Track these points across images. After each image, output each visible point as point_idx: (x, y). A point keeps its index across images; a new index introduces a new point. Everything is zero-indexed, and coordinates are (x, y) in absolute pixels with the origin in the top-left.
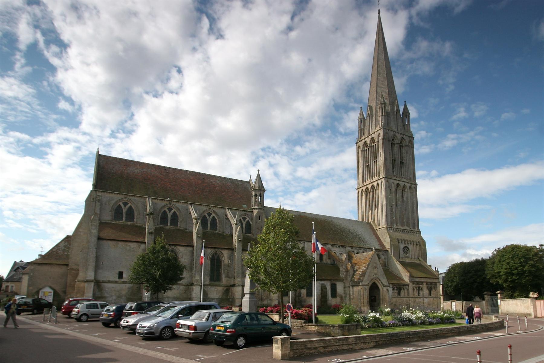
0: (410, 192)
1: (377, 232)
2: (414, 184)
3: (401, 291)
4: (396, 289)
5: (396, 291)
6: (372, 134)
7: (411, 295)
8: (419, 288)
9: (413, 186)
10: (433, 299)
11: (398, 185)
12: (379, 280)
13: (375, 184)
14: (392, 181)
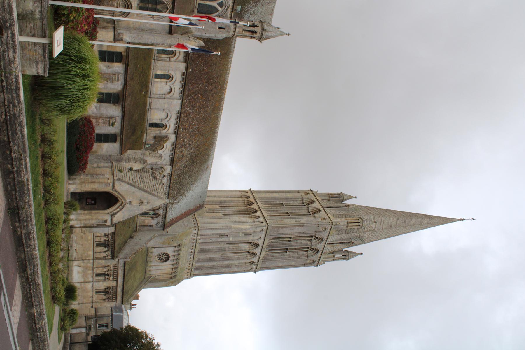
0: (246, 263)
1: (190, 216)
2: (256, 268)
3: (103, 248)
4: (107, 239)
5: (103, 239)
6: (324, 209)
7: (97, 262)
8: (108, 275)
9: (254, 266)
10: (91, 297)
11: (257, 245)
12: (121, 207)
13: (258, 214)
14: (263, 236)
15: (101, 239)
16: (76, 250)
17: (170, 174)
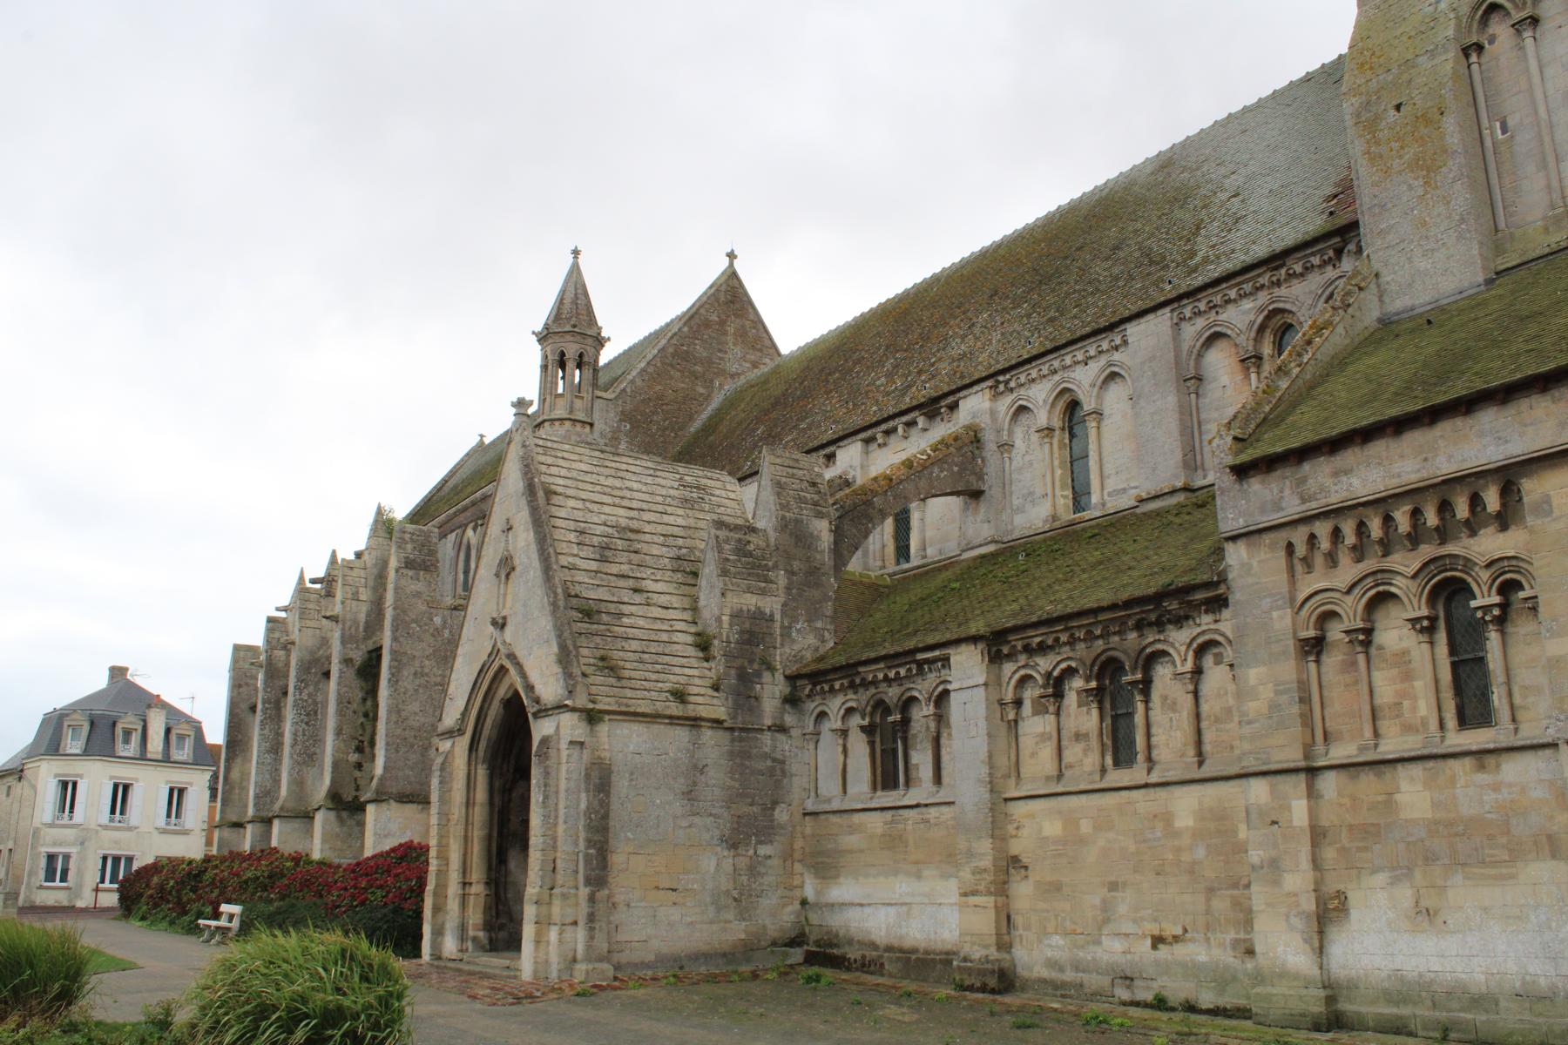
15: (1078, 737)
16: (1158, 941)
17: (990, 383)
